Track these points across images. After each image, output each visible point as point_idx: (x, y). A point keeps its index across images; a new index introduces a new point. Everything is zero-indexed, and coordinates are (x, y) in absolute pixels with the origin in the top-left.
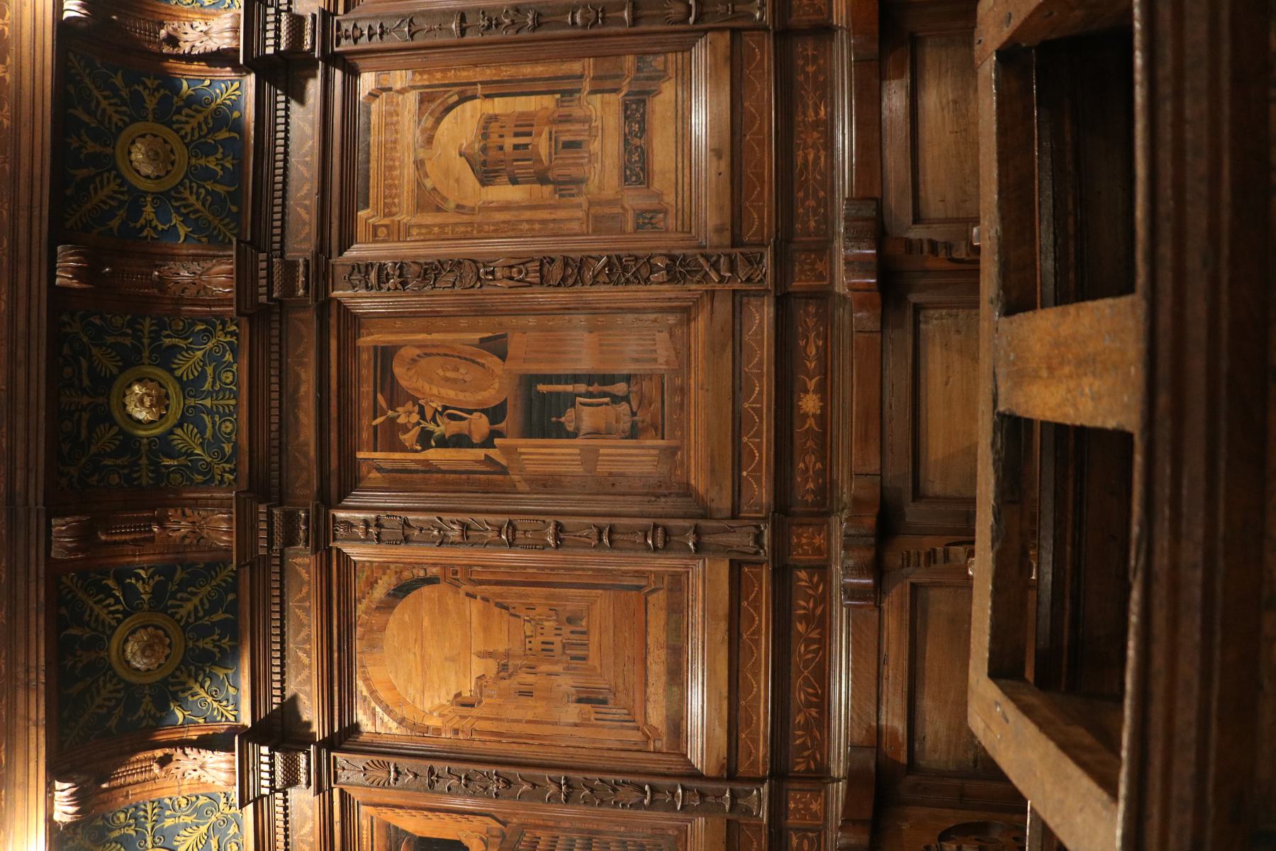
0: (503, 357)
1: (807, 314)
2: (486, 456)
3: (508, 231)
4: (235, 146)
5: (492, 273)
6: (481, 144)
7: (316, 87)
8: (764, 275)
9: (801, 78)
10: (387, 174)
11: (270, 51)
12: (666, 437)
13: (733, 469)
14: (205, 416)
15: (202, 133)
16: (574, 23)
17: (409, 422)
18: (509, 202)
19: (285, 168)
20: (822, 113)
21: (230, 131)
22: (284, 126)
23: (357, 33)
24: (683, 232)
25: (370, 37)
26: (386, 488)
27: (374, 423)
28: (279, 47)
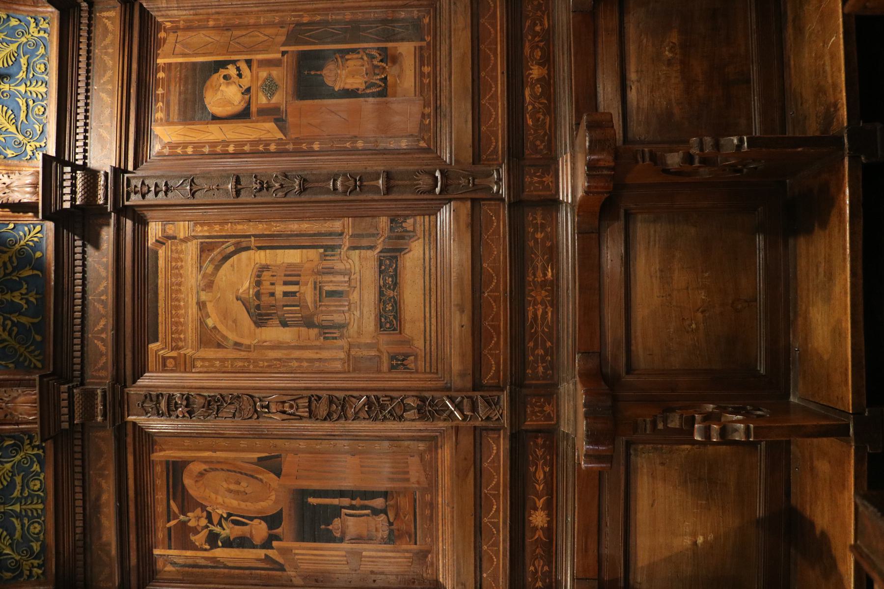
0: (278, 473)
1: (536, 444)
2: (266, 555)
3: (280, 367)
4: (37, 283)
5: (267, 407)
6: (255, 290)
8: (501, 415)
9: (532, 243)
10: (174, 312)
11: (67, 205)
12: (418, 543)
13: (475, 573)
14: (14, 520)
15: (8, 271)
16: (335, 189)
17: (198, 525)
18: (280, 342)
19: (84, 305)
20: (549, 274)
21: (33, 269)
22: (81, 262)
23: (145, 189)
24: (430, 372)
25: (156, 194)
26: (180, 580)
27: (168, 525)
28: (75, 201)
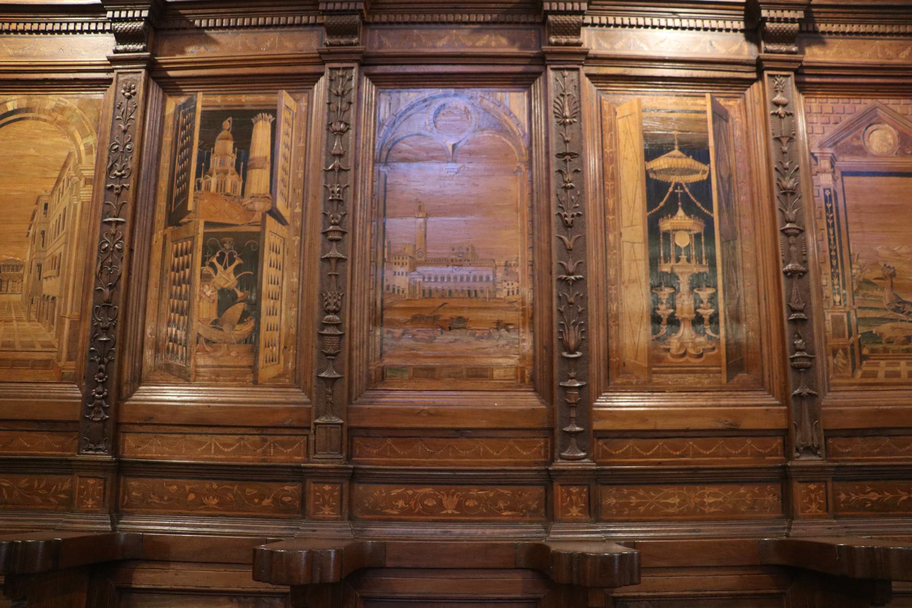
7: (499, 46)
11: (764, 13)
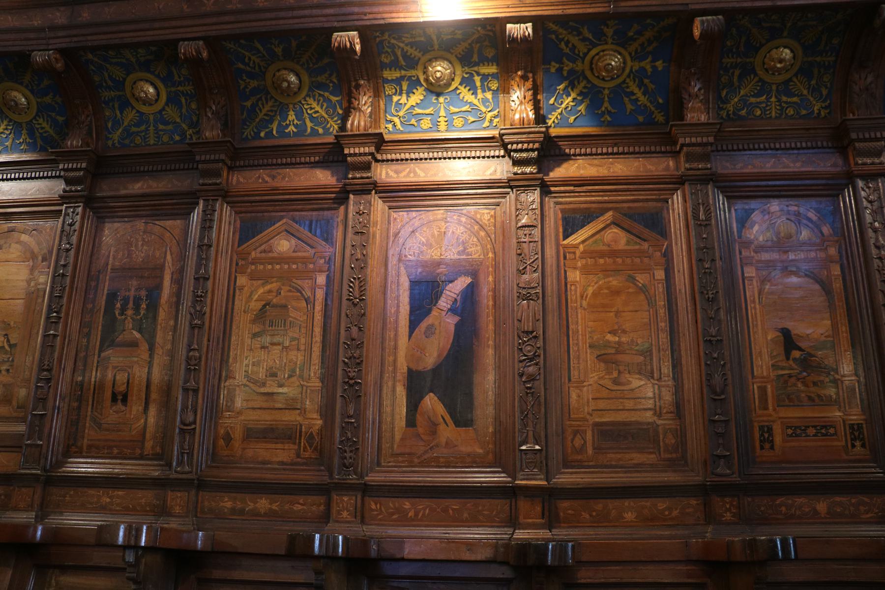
11: (346, 151)
14: (765, 97)
